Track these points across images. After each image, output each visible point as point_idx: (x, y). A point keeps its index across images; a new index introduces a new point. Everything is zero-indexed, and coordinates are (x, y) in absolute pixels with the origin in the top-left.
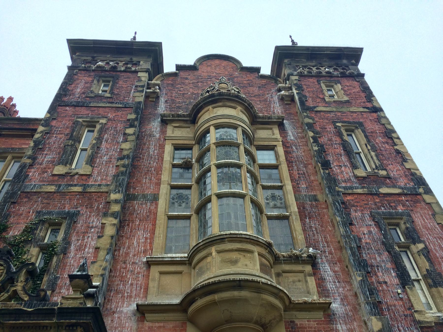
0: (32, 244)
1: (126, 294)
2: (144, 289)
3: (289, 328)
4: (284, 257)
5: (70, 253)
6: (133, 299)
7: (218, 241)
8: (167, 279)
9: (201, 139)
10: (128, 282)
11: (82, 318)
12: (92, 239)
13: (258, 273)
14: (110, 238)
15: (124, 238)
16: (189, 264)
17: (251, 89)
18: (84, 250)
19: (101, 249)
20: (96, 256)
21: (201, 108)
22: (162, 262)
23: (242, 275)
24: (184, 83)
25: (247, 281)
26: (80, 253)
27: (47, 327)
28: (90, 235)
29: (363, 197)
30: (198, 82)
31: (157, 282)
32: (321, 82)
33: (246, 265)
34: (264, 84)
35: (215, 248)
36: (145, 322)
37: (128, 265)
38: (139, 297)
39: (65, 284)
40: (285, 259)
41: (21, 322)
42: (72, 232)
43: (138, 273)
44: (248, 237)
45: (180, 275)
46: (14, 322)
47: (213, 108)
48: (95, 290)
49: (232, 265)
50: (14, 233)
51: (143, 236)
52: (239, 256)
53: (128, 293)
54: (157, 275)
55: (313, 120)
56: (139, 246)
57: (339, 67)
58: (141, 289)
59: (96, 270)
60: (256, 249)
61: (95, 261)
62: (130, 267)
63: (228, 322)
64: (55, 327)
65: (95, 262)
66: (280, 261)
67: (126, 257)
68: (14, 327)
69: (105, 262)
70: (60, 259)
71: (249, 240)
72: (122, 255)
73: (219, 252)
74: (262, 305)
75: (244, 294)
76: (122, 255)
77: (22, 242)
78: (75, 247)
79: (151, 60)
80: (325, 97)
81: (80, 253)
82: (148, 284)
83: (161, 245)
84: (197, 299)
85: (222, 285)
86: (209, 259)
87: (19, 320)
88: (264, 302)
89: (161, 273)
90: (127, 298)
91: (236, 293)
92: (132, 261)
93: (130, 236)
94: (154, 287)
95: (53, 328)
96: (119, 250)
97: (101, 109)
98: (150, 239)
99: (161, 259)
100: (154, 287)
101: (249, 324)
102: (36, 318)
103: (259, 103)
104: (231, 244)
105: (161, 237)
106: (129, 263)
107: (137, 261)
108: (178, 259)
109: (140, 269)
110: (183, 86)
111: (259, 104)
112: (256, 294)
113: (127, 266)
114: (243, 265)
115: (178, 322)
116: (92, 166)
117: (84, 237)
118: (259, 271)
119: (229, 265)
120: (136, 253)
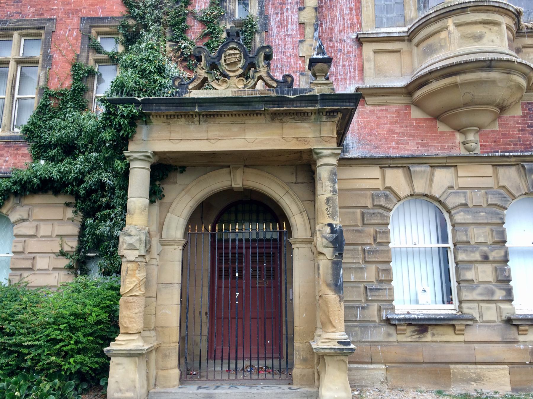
0: (226, 19)
1: (339, 77)
2: (359, 70)
3: (526, 110)
4: (527, 28)
5: (272, 30)
6: (348, 82)
7: (458, 11)
8: (384, 59)
10: (339, 63)
11: (344, 104)
12: (292, 12)
13: (507, 51)
14: (314, 10)
15: (324, 10)
16: (408, 40)
18: (287, 27)
19: (307, 25)
20: (303, 34)
22: (377, 39)
23: (491, 54)
25: (501, 60)
26: (283, 30)
27: (308, 113)
28: (289, 7)
31: (372, 63)
33: (492, 41)
35: (453, 21)
36: (366, 106)
37: (336, 44)
38: (355, 79)
39: (277, 66)
40: (529, 31)
41: (285, 108)
42: (267, 3)
43: (349, 53)
44: (497, 5)
45: (397, 55)
46: (278, 109)
49: (476, 41)
50: (201, 7)
51: (347, 5)
52: (486, 30)
53: (341, 75)
54: (372, 54)
56: (343, 19)
58: (355, 70)
59: (307, 50)
60: (505, 20)
61: (303, 39)
62: (338, 46)
63: (466, 105)
64: (315, 113)
65: (303, 41)
66: (521, 34)
67: (331, 33)
68: (275, 114)
69: (314, 41)
70: (263, 38)
71: (497, 9)
72: (326, 31)
73: (457, 25)
74: (509, 87)
75: (494, 75)
76: (326, 31)
77: (215, 18)
78: (276, 22)
81: (283, 30)
82: (363, 65)
83: (371, 17)
84: (432, 82)
85: (468, 66)
86: (443, 35)
87: (283, 107)
88: (512, 83)
89: (376, 52)
90: (341, 81)
91: (484, 75)
92: (339, 38)
93: (331, 6)
94: (370, 68)
95: (313, 114)
96: (322, 24)
98: (356, 9)
99: (375, 36)
100: (370, 68)
101: (489, 107)
102: (299, 105)
104: (474, 14)
105: (369, 6)
106: (337, 41)
107: (345, 38)
108: (395, 35)
109: (351, 47)
112: (505, 75)
113: (334, 44)
114: (488, 41)
115: (401, 106)
117: (282, 9)
118: (508, 48)
119: (472, 41)
120: (341, 28)
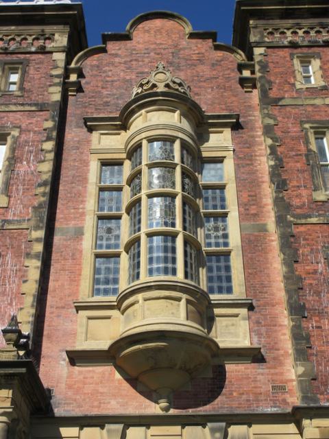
9: (134, 151)
17: (200, 68)
21: (133, 112)
24: (113, 64)
29: (317, 227)
30: (131, 61)
32: (295, 56)
34: (219, 59)
47: (148, 112)
48: (25, 340)
54: (85, 320)
55: (275, 119)
57: (324, 28)
79: (67, 29)
80: (296, 82)
97: (11, 114)
103: (210, 90)
110: (112, 68)
111: (210, 94)
116: (7, 196)
